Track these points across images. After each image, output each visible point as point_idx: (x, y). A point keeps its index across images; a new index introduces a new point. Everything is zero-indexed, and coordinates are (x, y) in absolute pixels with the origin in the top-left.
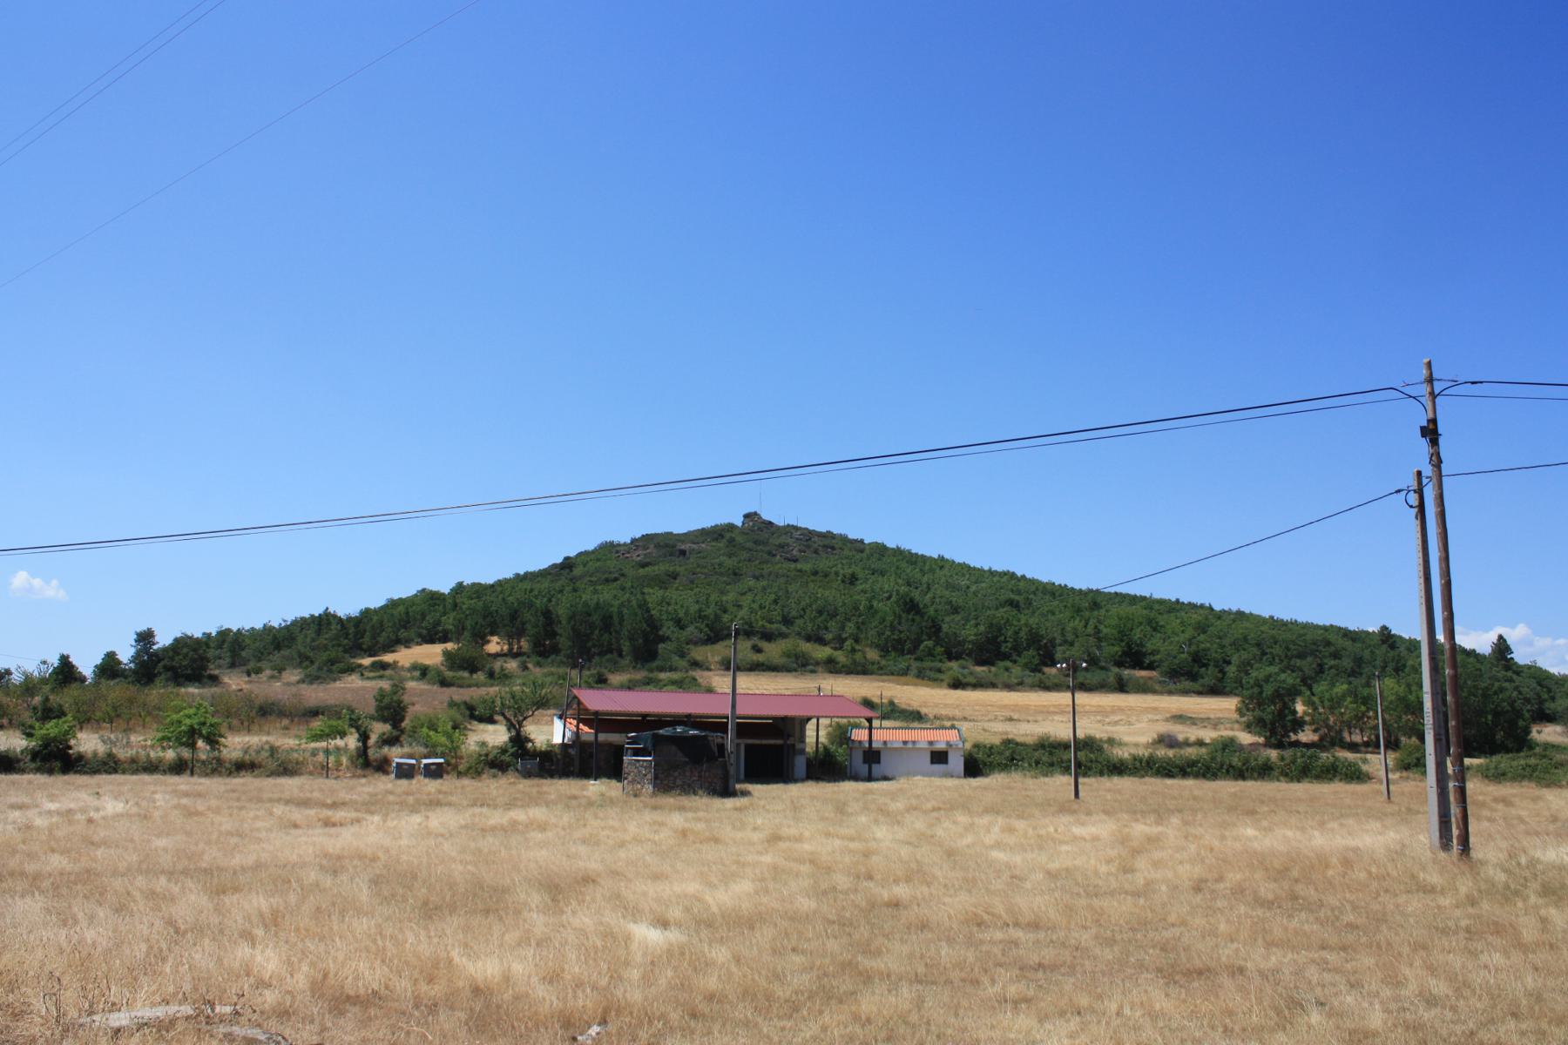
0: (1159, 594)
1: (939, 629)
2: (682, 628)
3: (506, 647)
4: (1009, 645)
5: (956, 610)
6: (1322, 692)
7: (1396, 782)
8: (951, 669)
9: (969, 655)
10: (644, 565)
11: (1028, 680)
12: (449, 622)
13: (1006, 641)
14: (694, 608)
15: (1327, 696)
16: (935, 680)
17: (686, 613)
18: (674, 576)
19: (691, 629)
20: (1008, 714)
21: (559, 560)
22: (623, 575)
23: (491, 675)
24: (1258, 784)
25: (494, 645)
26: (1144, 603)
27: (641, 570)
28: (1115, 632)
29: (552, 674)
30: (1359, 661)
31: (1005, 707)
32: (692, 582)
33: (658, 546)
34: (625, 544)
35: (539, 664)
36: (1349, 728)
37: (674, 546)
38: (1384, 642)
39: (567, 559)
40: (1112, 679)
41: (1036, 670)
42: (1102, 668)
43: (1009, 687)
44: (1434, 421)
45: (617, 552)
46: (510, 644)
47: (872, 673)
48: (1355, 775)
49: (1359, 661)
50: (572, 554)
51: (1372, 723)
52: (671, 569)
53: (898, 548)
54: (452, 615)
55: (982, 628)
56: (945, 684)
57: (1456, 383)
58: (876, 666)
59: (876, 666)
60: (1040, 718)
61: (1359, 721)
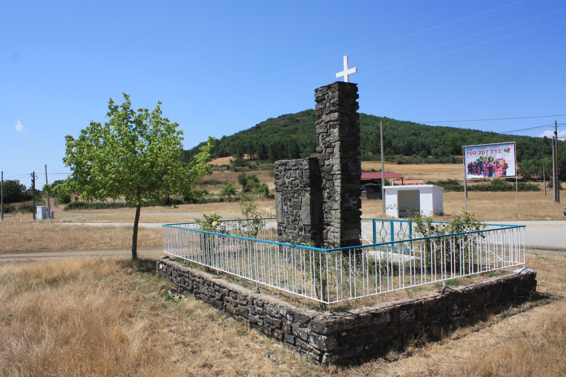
0: (462, 127)
1: (391, 144)
2: (306, 148)
3: (249, 158)
4: (415, 149)
5: (395, 137)
6: (524, 163)
7: (548, 191)
8: (397, 158)
9: (402, 152)
10: (286, 126)
11: (423, 161)
12: (227, 150)
13: (413, 147)
14: (308, 141)
15: (526, 164)
16: (392, 162)
17: (306, 143)
18: (297, 129)
19: (308, 148)
20: (419, 172)
21: (254, 125)
22: (279, 130)
23: (250, 167)
24: (509, 192)
25: (246, 157)
26: (458, 131)
27: (285, 128)
28: (451, 143)
29: (269, 166)
30: (536, 150)
31: (417, 170)
32: (304, 131)
33: (288, 119)
34: (276, 119)
35: (262, 163)
36: (533, 174)
37: (294, 119)
38: (545, 142)
39: (257, 125)
40: (451, 160)
41: (426, 157)
42: (447, 156)
43: (417, 163)
44: (556, 131)
45: (274, 121)
46: (251, 156)
47: (371, 160)
48: (536, 189)
49: (536, 150)
50: (258, 123)
51: (541, 172)
52: (296, 127)
53: (371, 115)
54: (228, 148)
55: (405, 143)
56: (396, 163)
57: (561, 124)
58: (372, 158)
59: (372, 158)
60: (429, 173)
61: (536, 171)
